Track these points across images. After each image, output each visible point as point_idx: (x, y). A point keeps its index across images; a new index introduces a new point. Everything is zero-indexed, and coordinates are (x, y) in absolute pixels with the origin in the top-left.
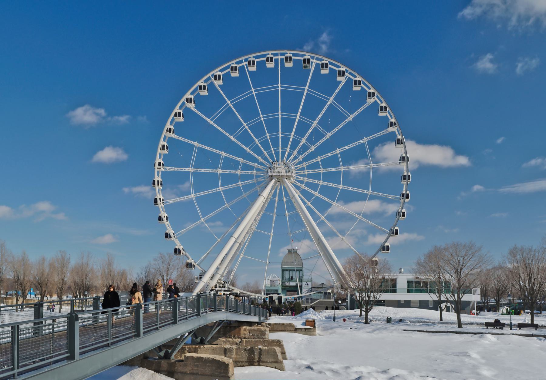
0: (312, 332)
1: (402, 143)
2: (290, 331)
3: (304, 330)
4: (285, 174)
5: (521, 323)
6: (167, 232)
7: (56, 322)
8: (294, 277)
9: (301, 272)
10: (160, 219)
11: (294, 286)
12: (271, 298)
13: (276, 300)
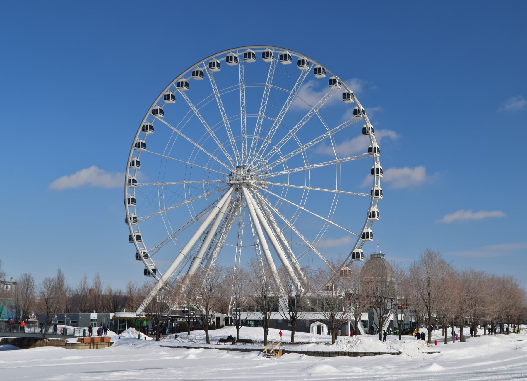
0: (77, 347)
1: (367, 133)
2: (62, 345)
3: (71, 345)
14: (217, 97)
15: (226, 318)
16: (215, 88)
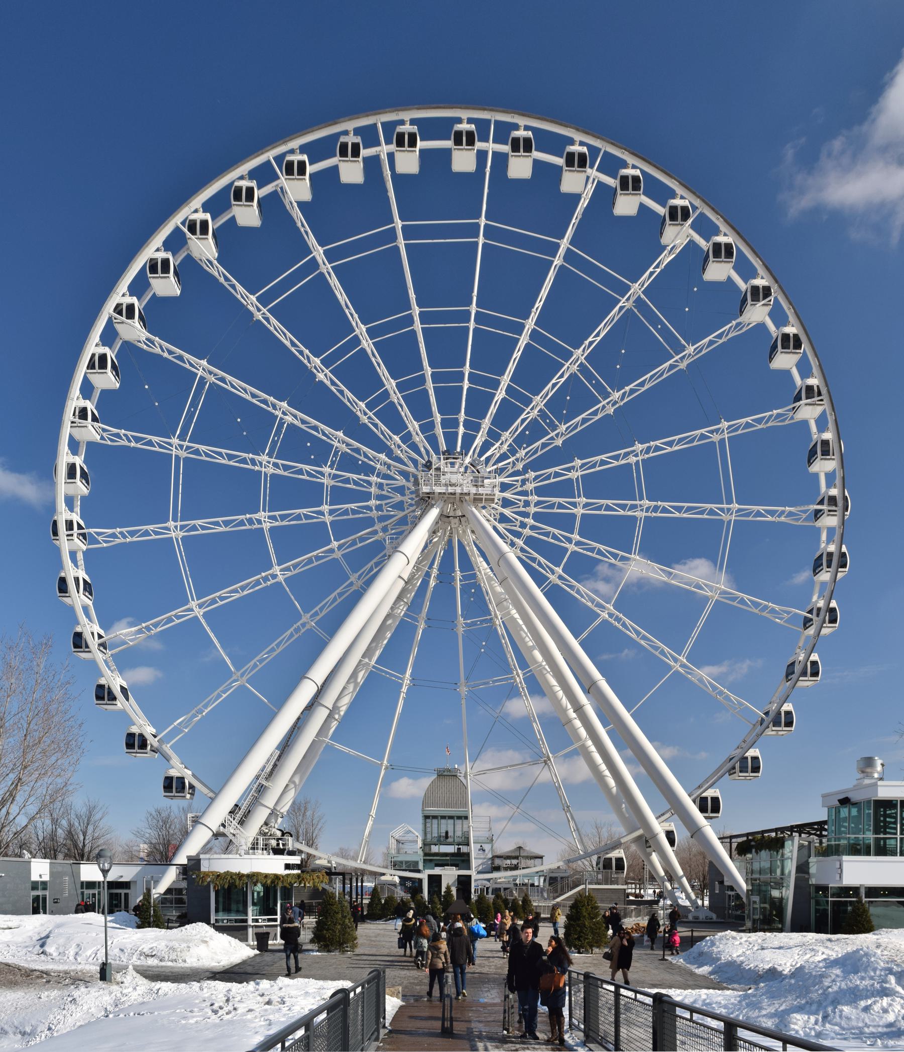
4: (473, 490)
5: (895, 930)
6: (102, 681)
8: (450, 834)
9: (465, 822)
10: (79, 641)
12: (435, 881)
13: (453, 885)
14: (676, 361)
15: (461, 878)
16: (735, 329)
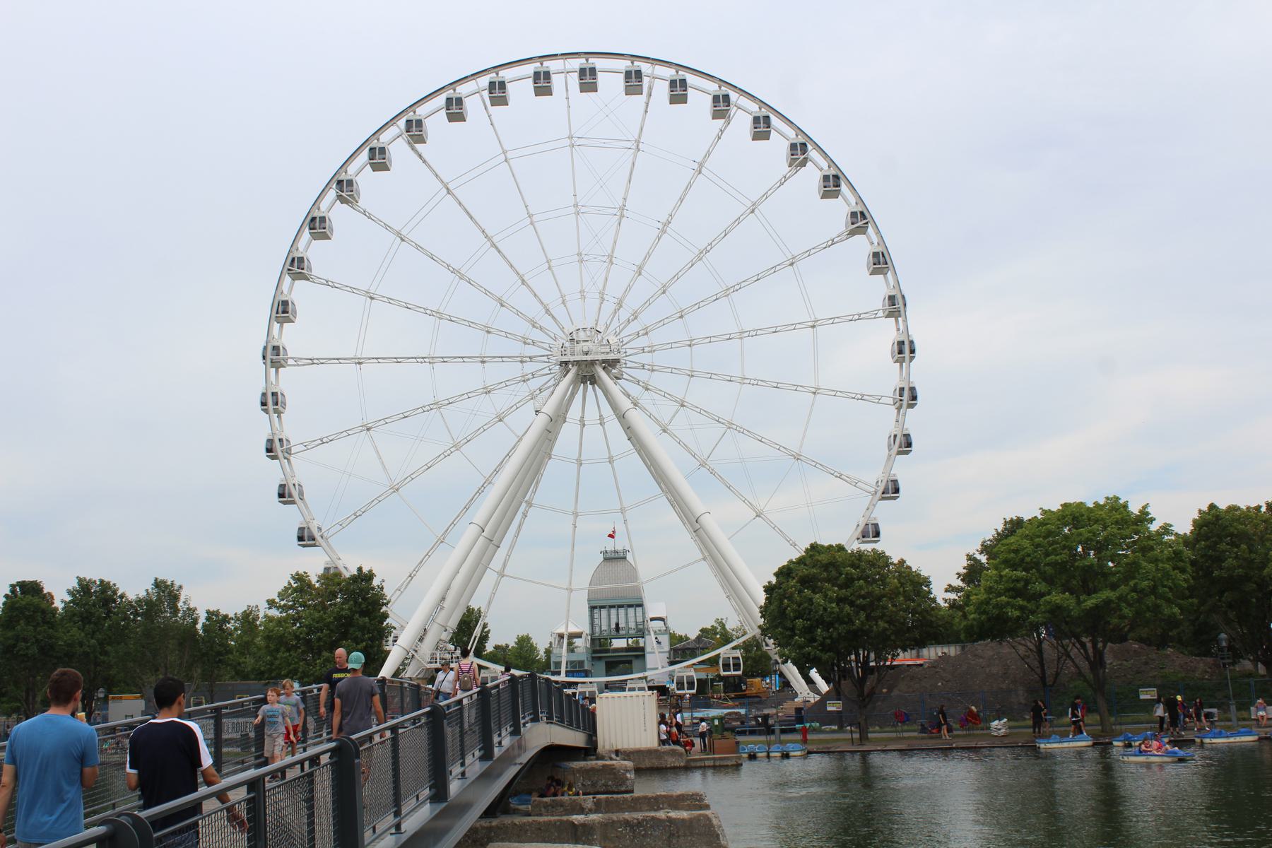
7: (318, 764)
8: (622, 625)
9: (639, 610)
11: (622, 648)
